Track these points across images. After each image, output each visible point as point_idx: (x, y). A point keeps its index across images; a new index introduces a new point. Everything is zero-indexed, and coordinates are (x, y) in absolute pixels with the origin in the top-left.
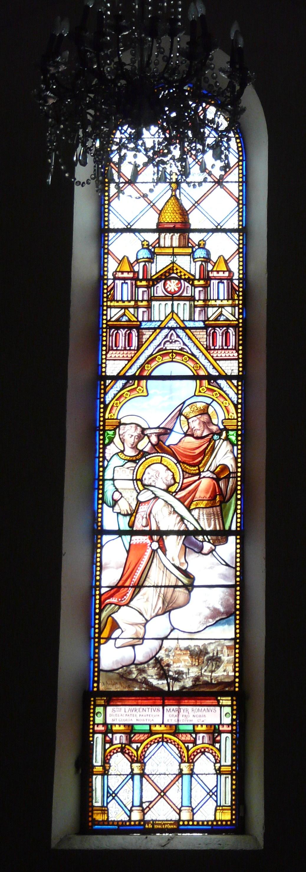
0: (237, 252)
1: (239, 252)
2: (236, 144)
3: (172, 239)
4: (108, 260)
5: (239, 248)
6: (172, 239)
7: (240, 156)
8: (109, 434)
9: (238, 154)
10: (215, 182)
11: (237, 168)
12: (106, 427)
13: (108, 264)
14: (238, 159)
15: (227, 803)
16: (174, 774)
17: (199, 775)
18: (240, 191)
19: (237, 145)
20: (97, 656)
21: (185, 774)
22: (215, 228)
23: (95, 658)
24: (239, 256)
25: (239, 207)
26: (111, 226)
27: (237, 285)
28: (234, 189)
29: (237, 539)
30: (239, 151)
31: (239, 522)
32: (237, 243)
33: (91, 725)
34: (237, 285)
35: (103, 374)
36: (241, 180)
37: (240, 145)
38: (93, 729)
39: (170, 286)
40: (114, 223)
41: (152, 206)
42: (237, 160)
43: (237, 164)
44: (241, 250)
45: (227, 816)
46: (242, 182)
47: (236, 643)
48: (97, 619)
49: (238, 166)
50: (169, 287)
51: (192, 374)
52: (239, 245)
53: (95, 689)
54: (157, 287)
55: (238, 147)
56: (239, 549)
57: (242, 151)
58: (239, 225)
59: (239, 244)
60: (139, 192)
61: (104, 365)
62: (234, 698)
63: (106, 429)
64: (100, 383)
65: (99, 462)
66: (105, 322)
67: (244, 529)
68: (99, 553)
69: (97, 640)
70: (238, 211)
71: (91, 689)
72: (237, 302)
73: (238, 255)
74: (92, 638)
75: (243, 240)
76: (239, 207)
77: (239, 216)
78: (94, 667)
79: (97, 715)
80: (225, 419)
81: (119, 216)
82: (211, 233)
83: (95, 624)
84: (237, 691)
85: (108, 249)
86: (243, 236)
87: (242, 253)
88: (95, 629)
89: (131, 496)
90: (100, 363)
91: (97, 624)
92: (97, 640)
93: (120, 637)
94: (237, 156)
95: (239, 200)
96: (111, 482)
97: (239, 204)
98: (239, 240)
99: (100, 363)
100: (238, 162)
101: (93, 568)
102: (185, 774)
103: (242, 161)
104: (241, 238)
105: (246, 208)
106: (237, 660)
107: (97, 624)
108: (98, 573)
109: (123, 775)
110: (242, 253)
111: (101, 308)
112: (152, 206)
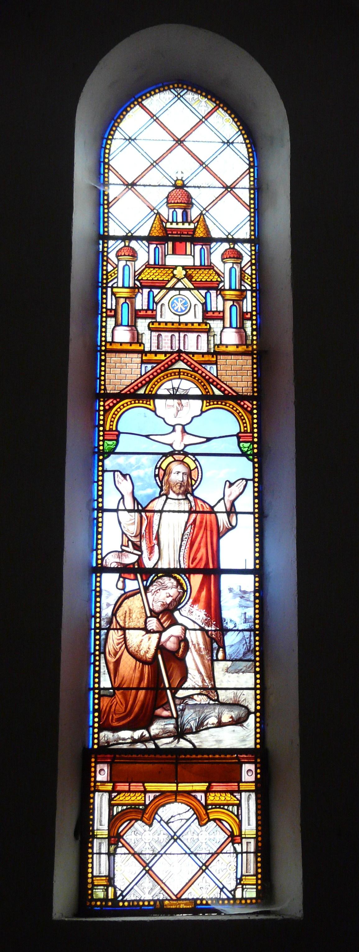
0: (249, 264)
2: (246, 149)
3: (101, 798)
5: (252, 259)
6: (101, 798)
7: (250, 162)
9: (249, 160)
14: (249, 165)
16: (209, 853)
17: (184, 852)
18: (251, 199)
20: (98, 610)
21: (103, 854)
22: (226, 237)
23: (98, 480)
24: (251, 268)
28: (245, 195)
29: (255, 577)
32: (249, 254)
33: (91, 782)
38: (92, 882)
41: (157, 164)
43: (248, 171)
49: (250, 173)
50: (176, 305)
51: (201, 394)
52: (251, 256)
54: (162, 305)
55: (249, 153)
58: (251, 235)
59: (252, 255)
65: (101, 355)
69: (103, 353)
70: (250, 220)
73: (250, 267)
77: (251, 226)
78: (100, 385)
79: (100, 773)
85: (107, 256)
89: (182, 173)
90: (98, 376)
92: (97, 691)
93: (222, 141)
94: (248, 162)
95: (251, 208)
97: (251, 213)
98: (251, 250)
99: (98, 376)
100: (249, 169)
102: (103, 854)
103: (253, 167)
104: (253, 248)
109: (226, 853)
112: (157, 164)
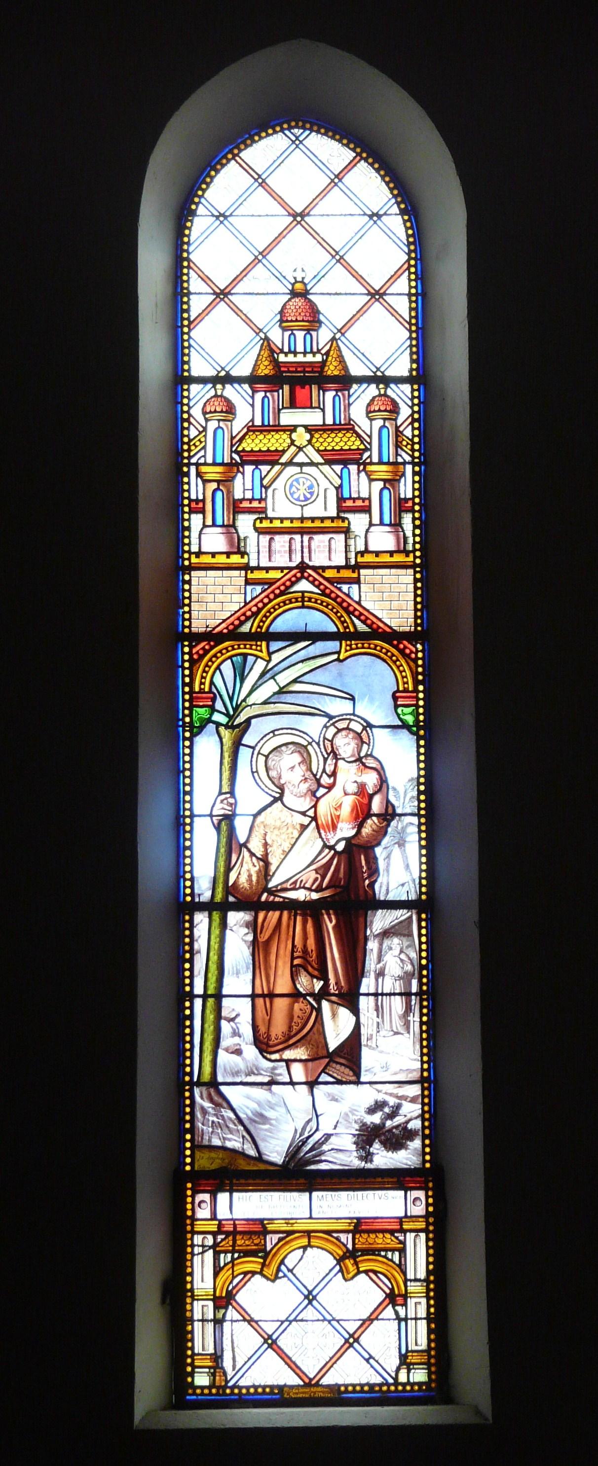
0: (410, 420)
1: (413, 418)
4: (189, 278)
8: (198, 714)
10: (369, 293)
11: (410, 427)
12: (196, 1361)
13: (190, 231)
15: (419, 1342)
19: (406, 232)
25: (409, 264)
26: (195, 373)
27: (408, 320)
30: (409, 244)
31: (421, 651)
34: (408, 320)
35: (186, 374)
36: (413, 291)
37: (410, 232)
39: (298, 489)
40: (198, 367)
42: (406, 257)
44: (416, 416)
45: (420, 1376)
46: (416, 295)
47: (430, 1357)
48: (189, 887)
50: (296, 491)
53: (188, 1168)
55: (408, 236)
56: (424, 871)
57: (414, 243)
60: (239, 313)
61: (185, 278)
62: (424, 916)
63: (196, 1364)
64: (184, 918)
66: (186, 502)
67: (428, 629)
68: (189, 872)
71: (181, 629)
72: (411, 558)
74: (181, 825)
75: (429, 1096)
76: (409, 264)
80: (398, 691)
81: (208, 357)
82: (367, 385)
83: (183, 661)
84: (425, 900)
86: (419, 390)
87: (418, 420)
88: (184, 669)
91: (187, 661)
96: (206, 1317)
101: (179, 883)
105: (423, 300)
106: (428, 1150)
107: (187, 661)
108: (187, 758)
110: (418, 420)
111: (182, 827)
112: (264, 257)
